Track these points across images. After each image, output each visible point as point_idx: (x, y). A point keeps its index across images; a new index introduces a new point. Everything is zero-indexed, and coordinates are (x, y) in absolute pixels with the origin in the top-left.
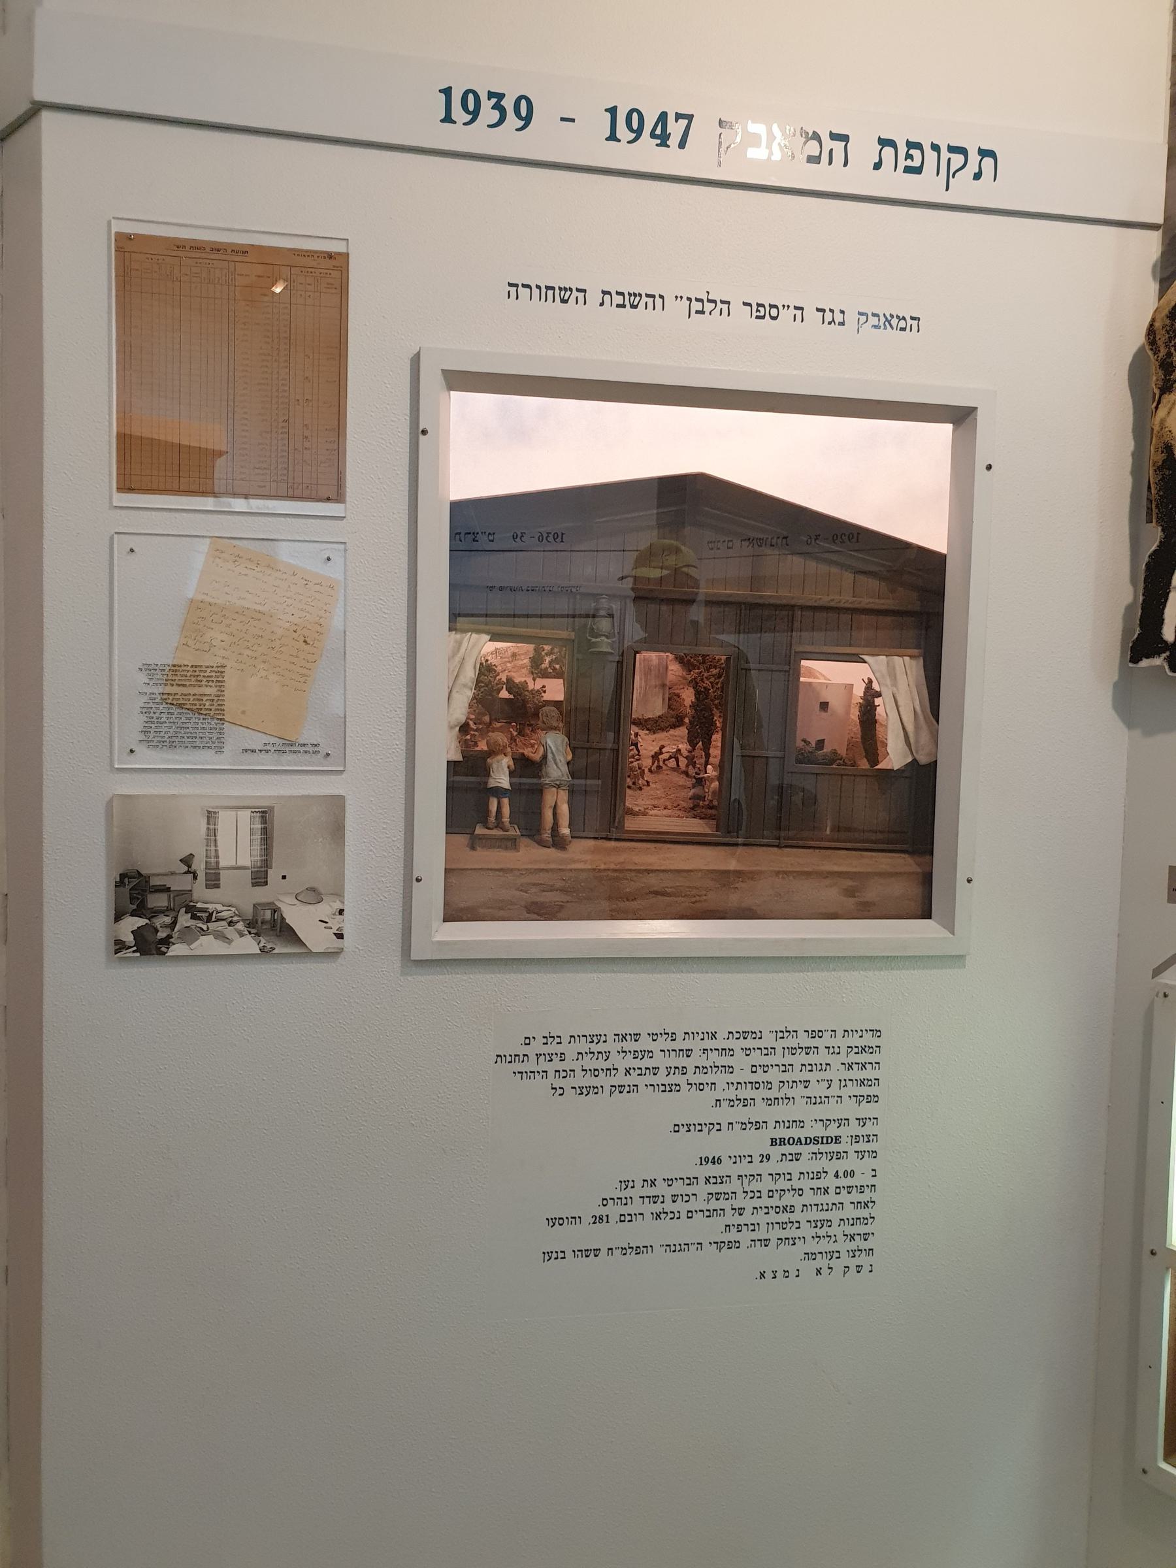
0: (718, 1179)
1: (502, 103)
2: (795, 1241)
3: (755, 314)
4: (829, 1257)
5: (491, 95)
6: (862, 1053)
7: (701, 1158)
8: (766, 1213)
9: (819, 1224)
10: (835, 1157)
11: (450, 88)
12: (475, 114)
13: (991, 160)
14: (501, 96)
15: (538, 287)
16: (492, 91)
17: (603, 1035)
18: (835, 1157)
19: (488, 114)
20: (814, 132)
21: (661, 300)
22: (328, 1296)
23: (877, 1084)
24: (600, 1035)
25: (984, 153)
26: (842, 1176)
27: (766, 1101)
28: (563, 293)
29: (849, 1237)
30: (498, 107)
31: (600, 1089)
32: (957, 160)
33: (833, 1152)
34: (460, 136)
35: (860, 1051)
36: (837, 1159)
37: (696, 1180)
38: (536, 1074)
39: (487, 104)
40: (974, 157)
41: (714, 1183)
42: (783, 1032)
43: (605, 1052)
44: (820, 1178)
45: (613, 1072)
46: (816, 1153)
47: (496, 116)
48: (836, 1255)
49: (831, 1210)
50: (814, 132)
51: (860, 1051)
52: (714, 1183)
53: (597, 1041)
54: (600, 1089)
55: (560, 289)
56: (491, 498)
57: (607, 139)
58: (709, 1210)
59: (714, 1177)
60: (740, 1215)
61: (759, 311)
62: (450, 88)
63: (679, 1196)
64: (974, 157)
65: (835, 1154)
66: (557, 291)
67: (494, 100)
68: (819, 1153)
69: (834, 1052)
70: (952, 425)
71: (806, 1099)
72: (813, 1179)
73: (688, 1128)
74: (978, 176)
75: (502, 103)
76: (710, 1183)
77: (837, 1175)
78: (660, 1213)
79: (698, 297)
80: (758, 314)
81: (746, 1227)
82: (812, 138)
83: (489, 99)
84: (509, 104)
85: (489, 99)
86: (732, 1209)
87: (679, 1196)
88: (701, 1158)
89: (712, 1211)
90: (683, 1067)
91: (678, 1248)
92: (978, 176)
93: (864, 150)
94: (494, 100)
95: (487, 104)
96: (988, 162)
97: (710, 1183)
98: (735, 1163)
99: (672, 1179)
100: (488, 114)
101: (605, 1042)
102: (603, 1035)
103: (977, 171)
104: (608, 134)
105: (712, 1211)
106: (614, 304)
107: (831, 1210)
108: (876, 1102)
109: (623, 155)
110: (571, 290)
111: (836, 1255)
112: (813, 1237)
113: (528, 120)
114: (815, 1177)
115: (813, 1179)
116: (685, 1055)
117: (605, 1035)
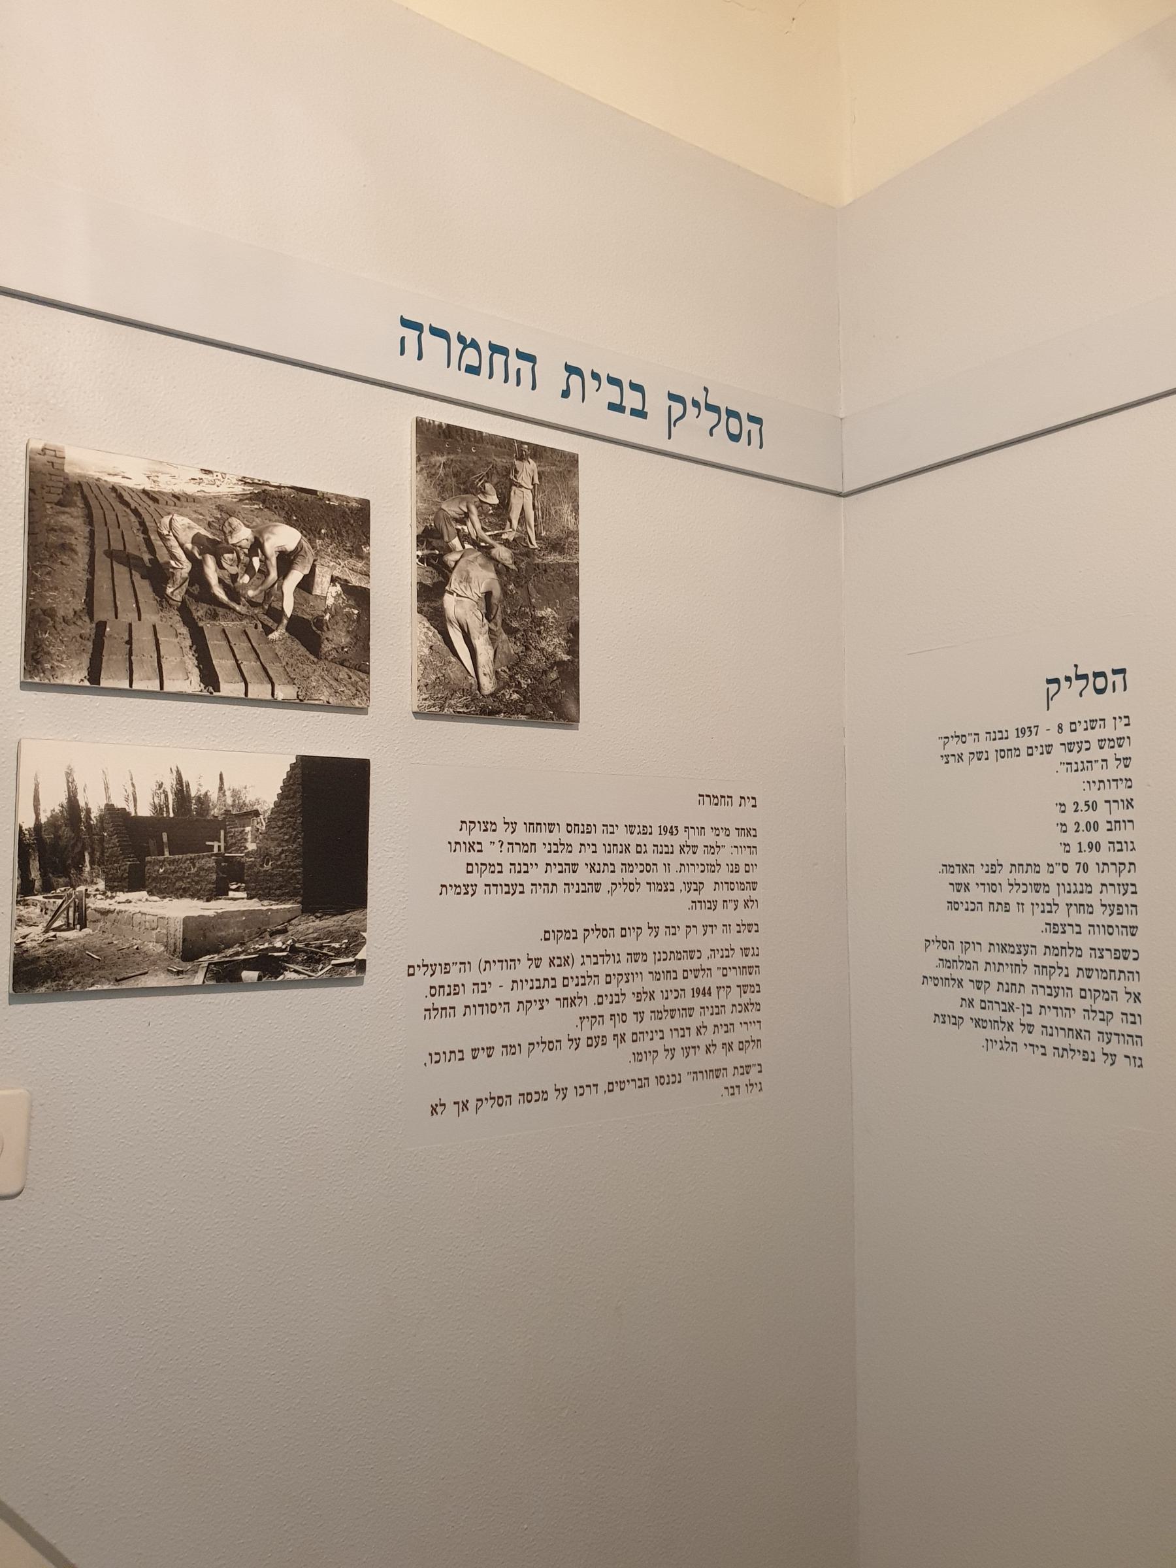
3: (443, 971)
4: (1123, 891)
8: (1126, 725)
9: (1076, 748)
10: (1116, 911)
16: (1115, 668)
18: (1116, 911)
19: (1028, 733)
22: (237, 1075)
23: (980, 908)
25: (1131, 864)
27: (454, 888)
29: (649, 994)
32: (1122, 867)
33: (1114, 905)
38: (538, 887)
39: (1027, 730)
40: (1127, 865)
41: (478, 851)
43: (512, 885)
44: (458, 993)
46: (429, 1010)
47: (1029, 733)
48: (1131, 889)
49: (603, 871)
52: (478, 851)
59: (478, 843)
60: (1126, 766)
63: (1126, 739)
64: (1127, 865)
65: (1116, 907)
66: (1129, 929)
68: (434, 1009)
69: (1076, 891)
71: (974, 736)
72: (449, 994)
74: (1129, 871)
76: (474, 850)
78: (575, 998)
81: (1116, 804)
87: (1126, 739)
91: (1080, 767)
92: (1129, 871)
95: (1027, 730)
96: (1132, 867)
97: (474, 850)
99: (624, 1082)
106: (457, 1059)
107: (603, 871)
108: (1090, 892)
111: (1131, 889)
114: (452, 992)
115: (449, 994)
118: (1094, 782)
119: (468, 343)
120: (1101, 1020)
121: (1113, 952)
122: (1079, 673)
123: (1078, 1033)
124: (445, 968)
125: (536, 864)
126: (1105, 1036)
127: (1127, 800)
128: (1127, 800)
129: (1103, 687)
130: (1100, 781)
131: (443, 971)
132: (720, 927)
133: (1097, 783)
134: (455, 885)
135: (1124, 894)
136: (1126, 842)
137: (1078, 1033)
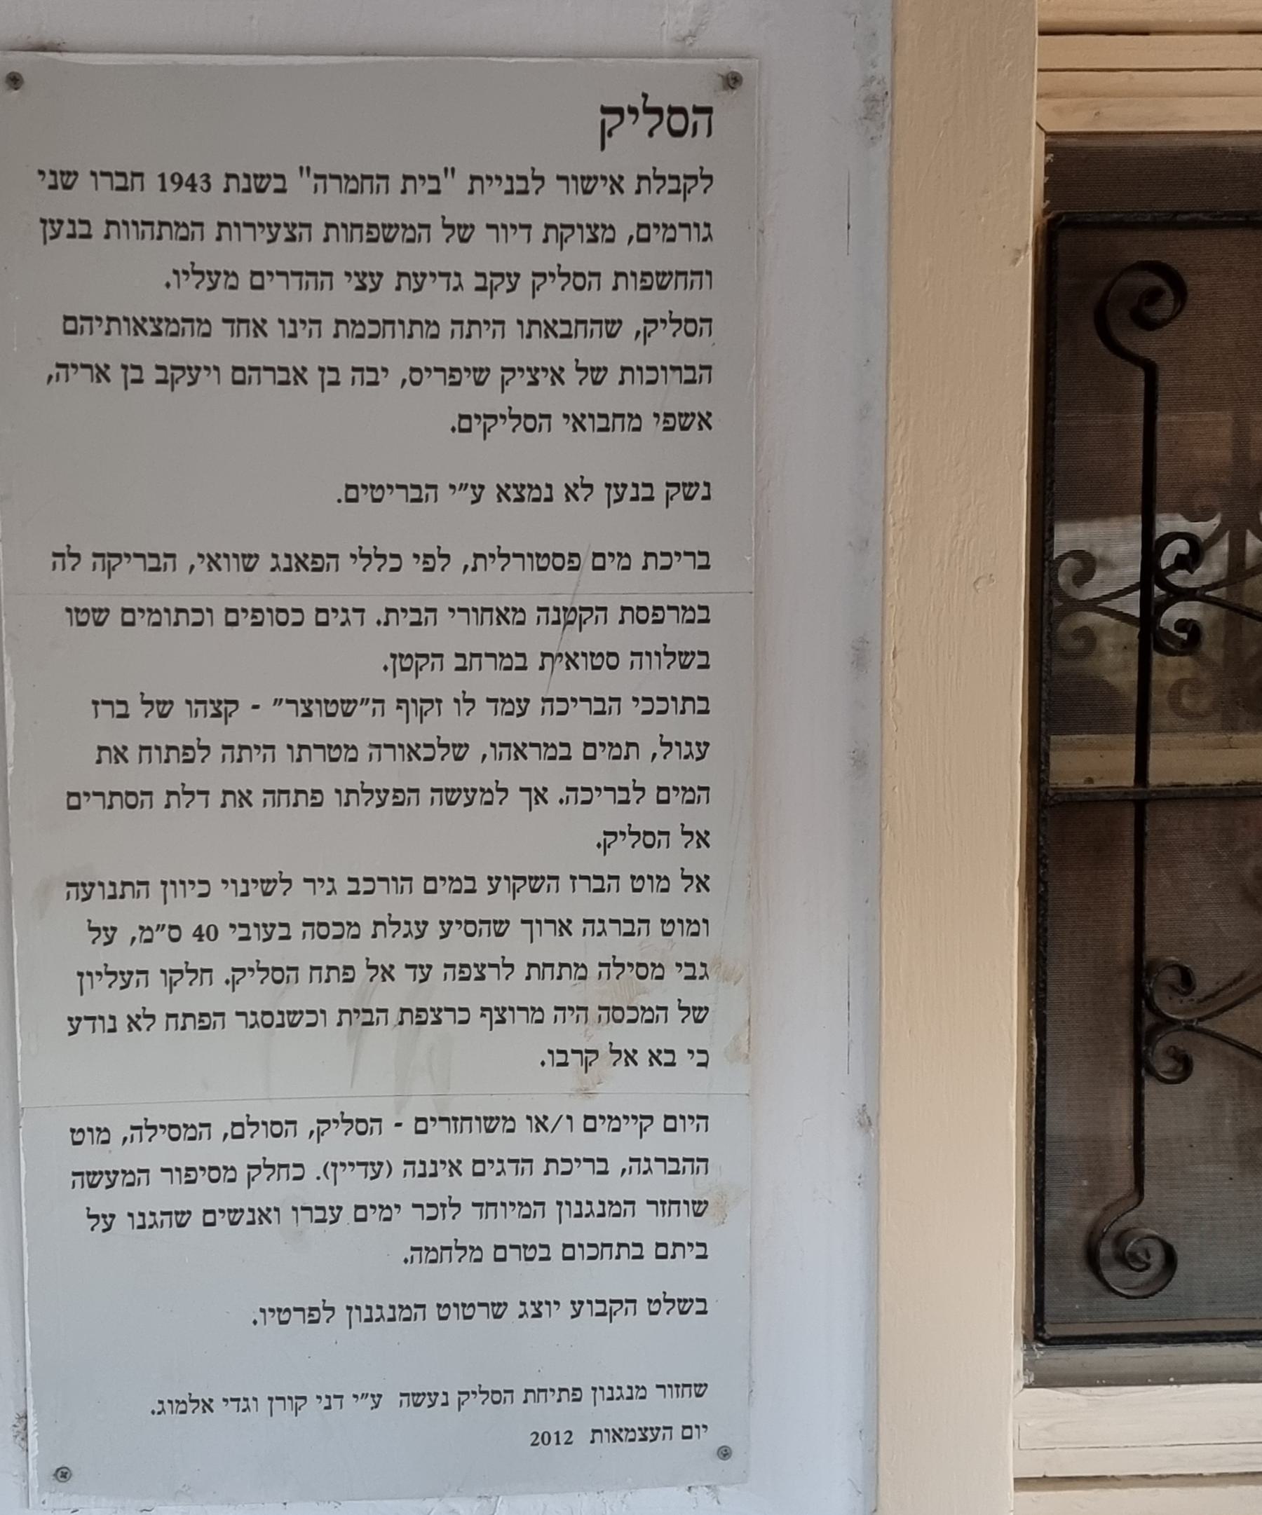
0: (638, 1433)
2: (537, 376)
3: (458, 976)
6: (296, 383)
7: (162, 176)
10: (390, 800)
17: (701, 484)
18: (390, 800)
24: (60, 222)
33: (386, 791)
35: (291, 379)
36: (395, 804)
37: (707, 372)
42: (626, 789)
45: (71, 561)
51: (291, 379)
56: (1032, 497)
65: (391, 794)
73: (533, 377)
89: (611, 419)
90: (575, 1389)
98: (328, 1408)
101: (707, 498)
102: (701, 484)
105: (611, 419)
112: (353, 556)
116: (691, 1213)
117: (445, 1394)
122: (648, 105)
131: (365, 237)
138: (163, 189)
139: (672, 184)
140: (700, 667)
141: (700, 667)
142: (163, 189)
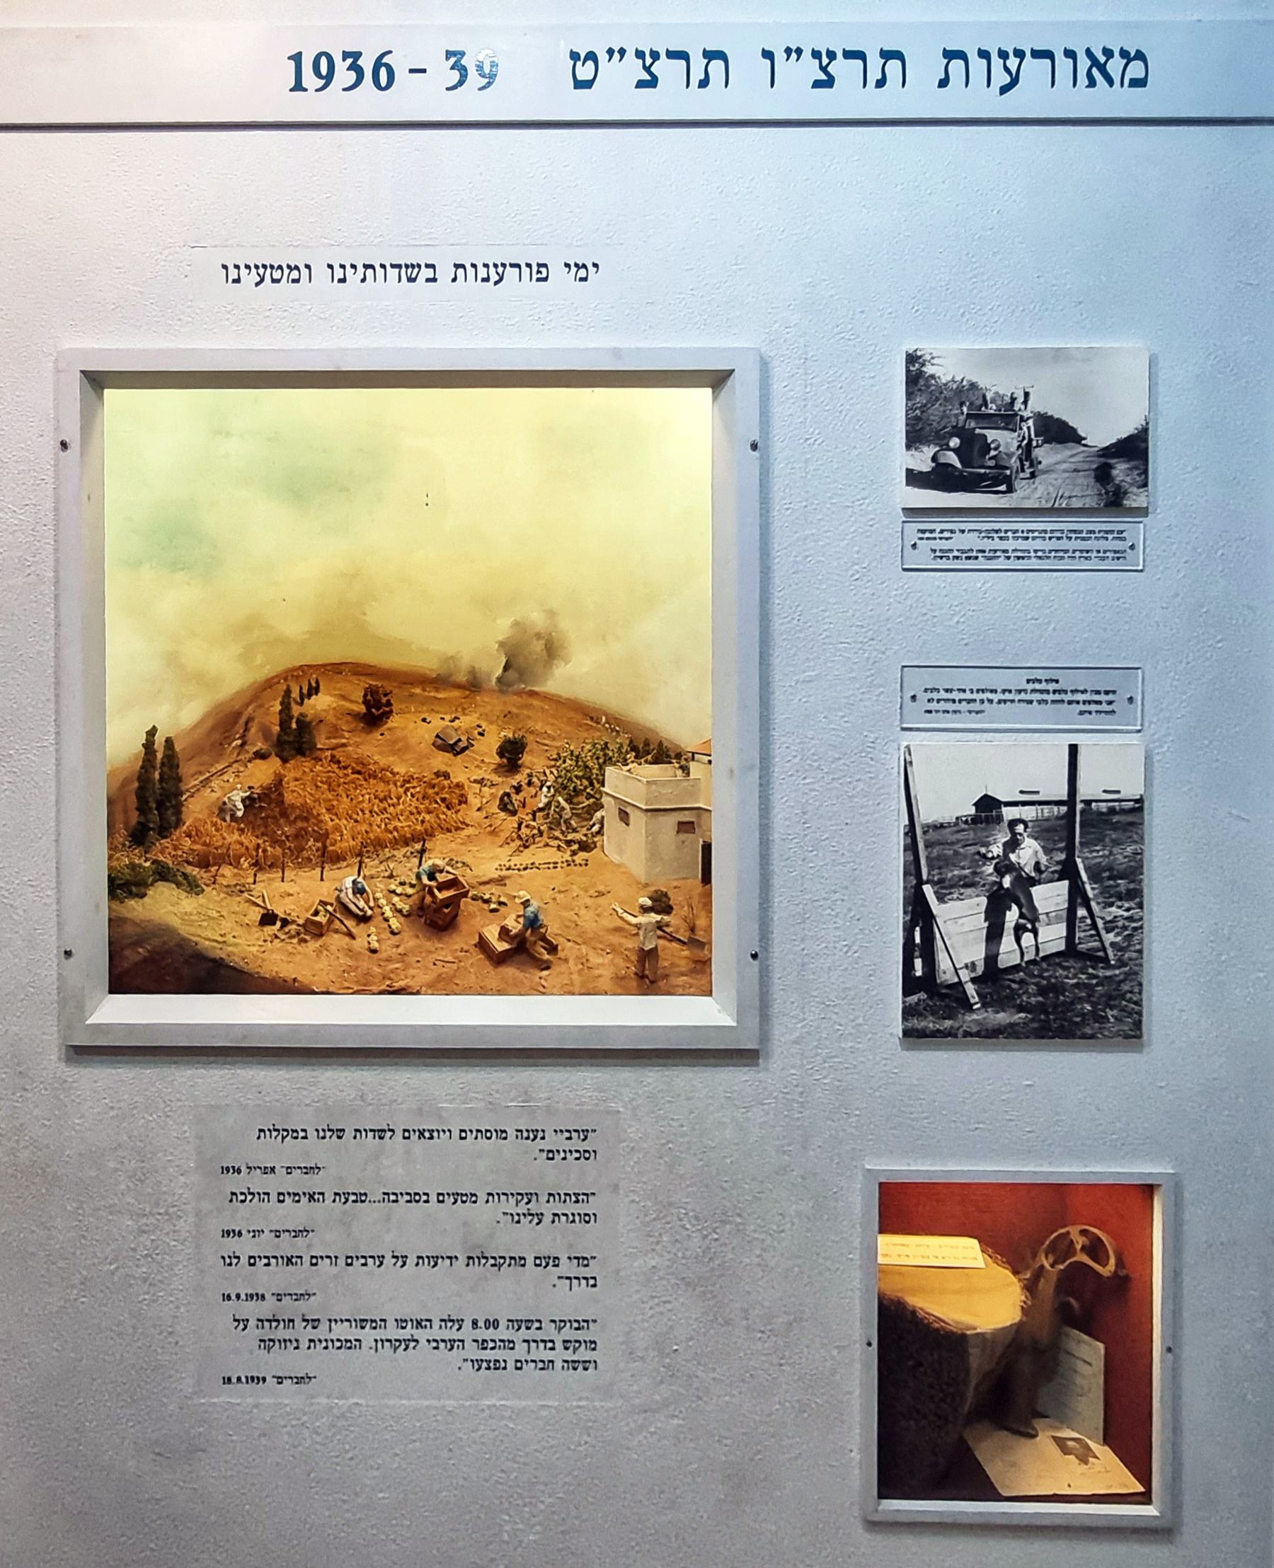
1: (359, 63)
3: (535, 276)
5: (346, 55)
7: (297, 58)
11: (300, 53)
12: (329, 78)
13: (721, 63)
14: (357, 55)
15: (529, 265)
16: (347, 50)
19: (344, 75)
20: (1138, 51)
21: (473, 270)
26: (483, 1326)
27: (574, 269)
28: (410, 270)
30: (355, 67)
31: (305, 272)
34: (313, 105)
39: (341, 66)
47: (352, 76)
50: (1138, 51)
53: (497, 278)
54: (305, 272)
55: (407, 266)
57: (291, 90)
58: (542, 1361)
61: (541, 272)
62: (300, 53)
66: (404, 269)
67: (350, 61)
70: (106, 391)
75: (359, 63)
77: (475, 1323)
79: (428, 263)
80: (539, 276)
82: (1135, 58)
83: (344, 60)
84: (367, 64)
85: (344, 60)
86: (235, 1320)
88: (297, 58)
93: (925, 66)
94: (350, 61)
95: (341, 66)
100: (344, 75)
103: (943, 77)
104: (293, 84)
106: (230, 280)
109: (313, 105)
110: (419, 266)
113: (491, 79)
118: (353, 266)
119: (1132, 55)
120: (492, 1265)
121: (535, 269)
123: (1095, 62)
124: (539, 272)
125: (595, 265)
126: (515, 1324)
127: (1089, 53)
128: (1089, 53)
129: (591, 78)
130: (366, 267)
131: (535, 276)
132: (399, 1133)
133: (361, 269)
134: (576, 265)
135: (1004, 90)
136: (474, 266)
137: (1095, 62)
138: (298, 87)
139: (492, 1261)
140: (428, 280)
141: (428, 280)
142: (298, 87)
